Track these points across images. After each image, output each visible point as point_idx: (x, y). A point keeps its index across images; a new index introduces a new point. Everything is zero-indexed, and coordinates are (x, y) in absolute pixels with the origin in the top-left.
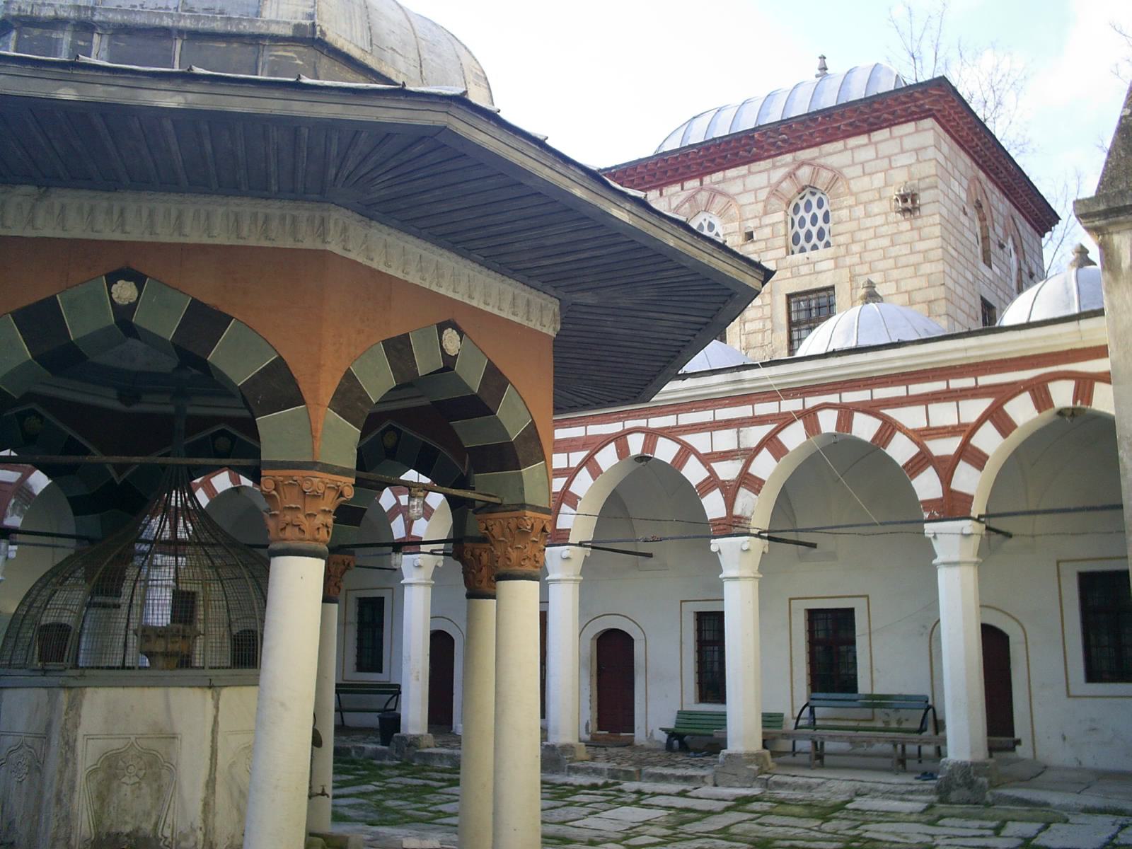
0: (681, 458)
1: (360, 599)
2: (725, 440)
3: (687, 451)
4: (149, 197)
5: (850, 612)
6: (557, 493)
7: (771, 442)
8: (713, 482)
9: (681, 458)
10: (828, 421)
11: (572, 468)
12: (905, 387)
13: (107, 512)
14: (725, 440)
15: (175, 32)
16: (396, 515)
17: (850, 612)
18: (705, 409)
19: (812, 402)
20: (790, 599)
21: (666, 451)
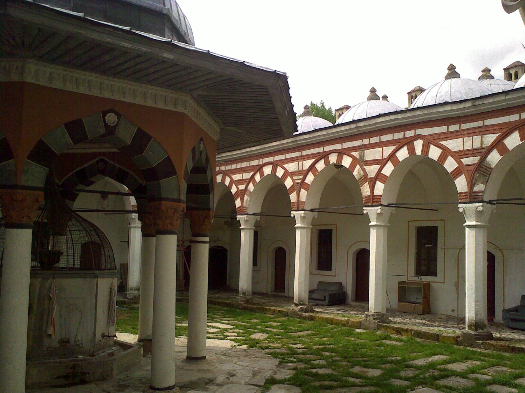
0: (443, 158)
1: (319, 230)
2: (468, 143)
3: (446, 153)
4: (71, 70)
5: (436, 228)
6: (372, 178)
7: (498, 144)
8: (365, 178)
9: (443, 158)
10: (418, 145)
11: (304, 170)
12: (368, 139)
13: (76, 376)
14: (468, 143)
15: (317, 319)
16: (232, 185)
17: (436, 228)
18: (319, 147)
19: (410, 134)
20: (409, 222)
21: (434, 153)
